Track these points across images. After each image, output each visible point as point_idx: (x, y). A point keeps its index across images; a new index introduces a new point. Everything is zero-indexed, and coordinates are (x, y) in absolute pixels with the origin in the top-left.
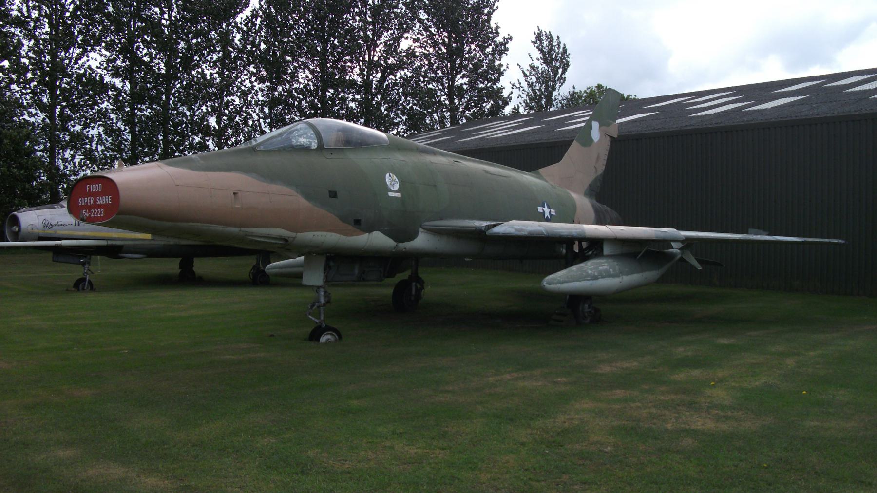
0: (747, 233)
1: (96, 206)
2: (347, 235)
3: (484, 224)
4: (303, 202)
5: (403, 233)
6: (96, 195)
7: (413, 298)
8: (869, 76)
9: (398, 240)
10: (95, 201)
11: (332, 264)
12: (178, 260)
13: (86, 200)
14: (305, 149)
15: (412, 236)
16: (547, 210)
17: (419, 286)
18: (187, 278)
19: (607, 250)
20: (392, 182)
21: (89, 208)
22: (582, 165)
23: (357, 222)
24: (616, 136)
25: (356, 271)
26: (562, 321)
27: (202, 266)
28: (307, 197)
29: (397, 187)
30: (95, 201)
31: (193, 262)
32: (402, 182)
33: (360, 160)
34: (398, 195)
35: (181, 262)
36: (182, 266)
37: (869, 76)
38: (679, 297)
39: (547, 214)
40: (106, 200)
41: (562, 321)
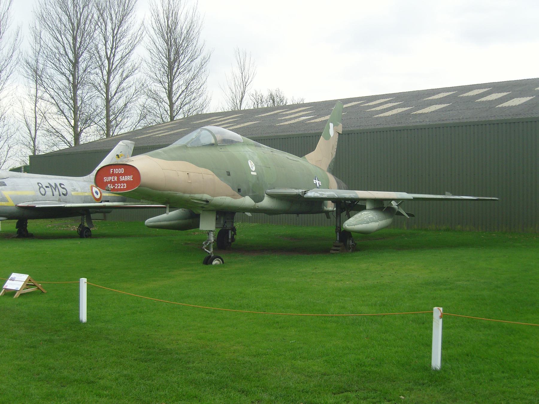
0: (444, 194)
1: (119, 182)
3: (301, 191)
4: (217, 178)
5: (258, 199)
6: (118, 175)
7: (230, 241)
8: (486, 90)
10: (118, 179)
11: (218, 217)
12: (17, 221)
13: (110, 178)
15: (261, 199)
16: (317, 182)
17: (233, 233)
20: (252, 166)
22: (323, 154)
23: (239, 190)
24: (341, 133)
25: (222, 222)
27: (33, 226)
28: (218, 175)
29: (254, 169)
30: (118, 179)
32: (256, 165)
33: (232, 150)
34: (255, 174)
35: (18, 223)
37: (486, 90)
38: (407, 231)
39: (318, 185)
40: (129, 178)
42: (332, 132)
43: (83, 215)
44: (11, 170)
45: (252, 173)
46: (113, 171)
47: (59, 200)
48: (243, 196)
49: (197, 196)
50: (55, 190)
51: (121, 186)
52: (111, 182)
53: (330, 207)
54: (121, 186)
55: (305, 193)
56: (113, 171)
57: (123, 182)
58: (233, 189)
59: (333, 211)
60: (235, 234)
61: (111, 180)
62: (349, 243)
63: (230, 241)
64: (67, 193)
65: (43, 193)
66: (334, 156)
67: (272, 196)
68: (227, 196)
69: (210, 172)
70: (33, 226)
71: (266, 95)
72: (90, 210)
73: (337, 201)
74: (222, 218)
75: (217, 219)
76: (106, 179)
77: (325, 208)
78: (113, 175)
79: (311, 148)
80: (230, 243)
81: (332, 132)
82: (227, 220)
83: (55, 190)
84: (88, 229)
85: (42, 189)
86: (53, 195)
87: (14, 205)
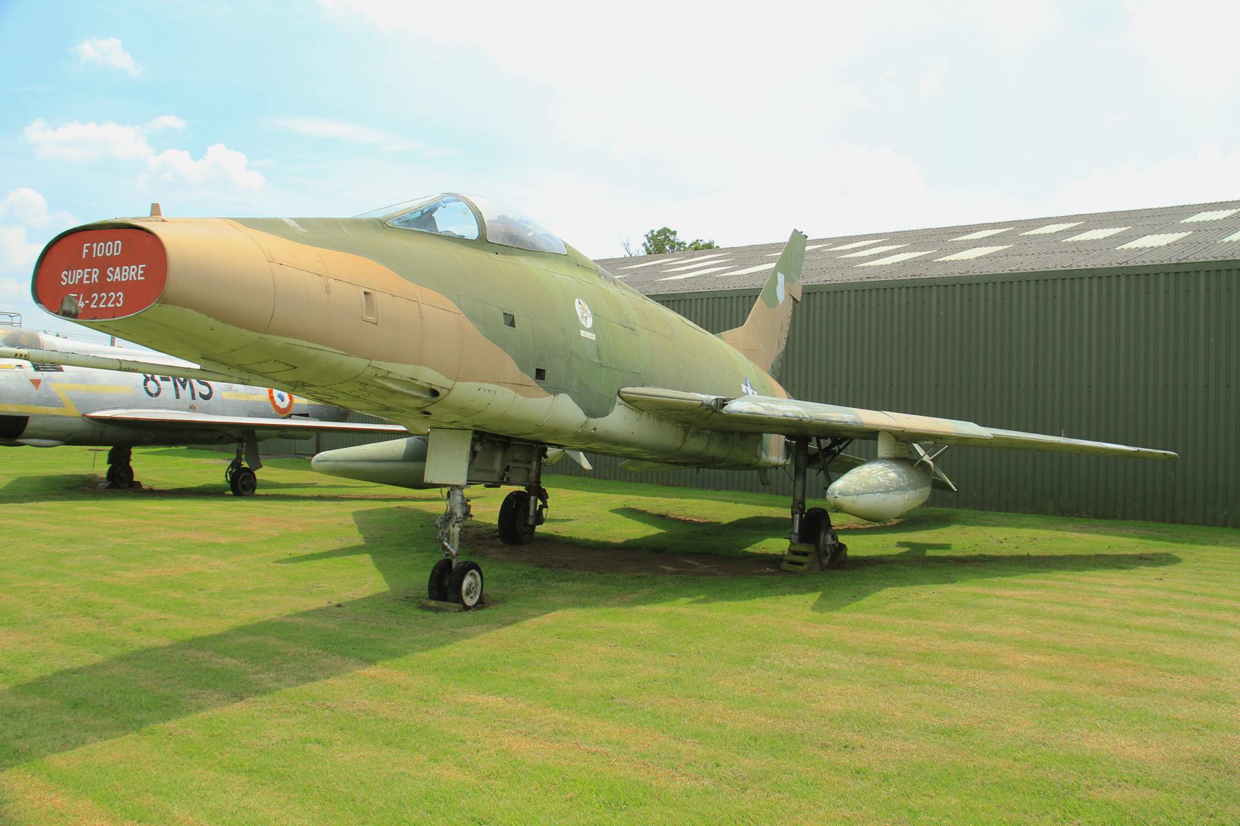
1: (104, 285)
2: (526, 395)
6: (104, 263)
9: (590, 414)
10: (103, 276)
11: (478, 448)
13: (79, 275)
14: (461, 240)
15: (605, 413)
17: (540, 503)
18: (121, 482)
19: (883, 449)
21: (85, 290)
22: (767, 325)
23: (540, 374)
25: (497, 466)
26: (801, 564)
27: (147, 464)
29: (589, 323)
30: (103, 276)
31: (130, 453)
32: (595, 315)
34: (592, 336)
35: (111, 454)
36: (112, 459)
40: (133, 273)
41: (801, 564)
42: (781, 294)
43: (240, 440)
44: (612, 511)
45: (583, 333)
46: (90, 249)
47: (192, 408)
48: (555, 391)
49: (404, 370)
50: (184, 387)
51: (100, 299)
52: (79, 288)
53: (774, 450)
54: (100, 299)
55: (723, 403)
56: (90, 249)
57: (117, 286)
58: (523, 367)
59: (784, 466)
60: (545, 505)
61: (81, 279)
62: (825, 541)
63: (531, 522)
64: (211, 393)
65: (154, 391)
66: (782, 348)
67: (631, 402)
68: (498, 383)
69: (452, 305)
70: (147, 464)
71: (646, 240)
72: (257, 432)
73: (799, 436)
74: (498, 456)
75: (473, 454)
76: (70, 278)
77: (763, 455)
78: (91, 262)
79: (737, 320)
80: (533, 527)
81: (781, 294)
82: (512, 465)
83: (184, 387)
84: (250, 473)
85: (151, 384)
86: (178, 396)
87: (79, 414)
